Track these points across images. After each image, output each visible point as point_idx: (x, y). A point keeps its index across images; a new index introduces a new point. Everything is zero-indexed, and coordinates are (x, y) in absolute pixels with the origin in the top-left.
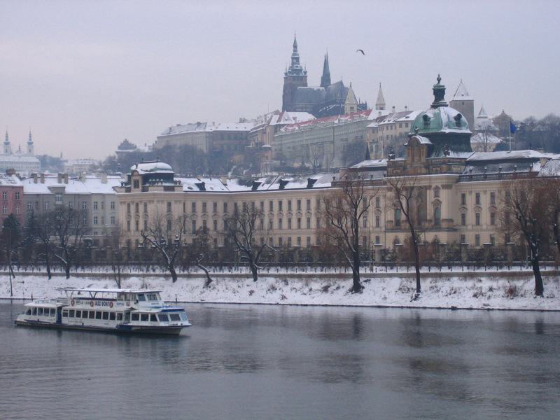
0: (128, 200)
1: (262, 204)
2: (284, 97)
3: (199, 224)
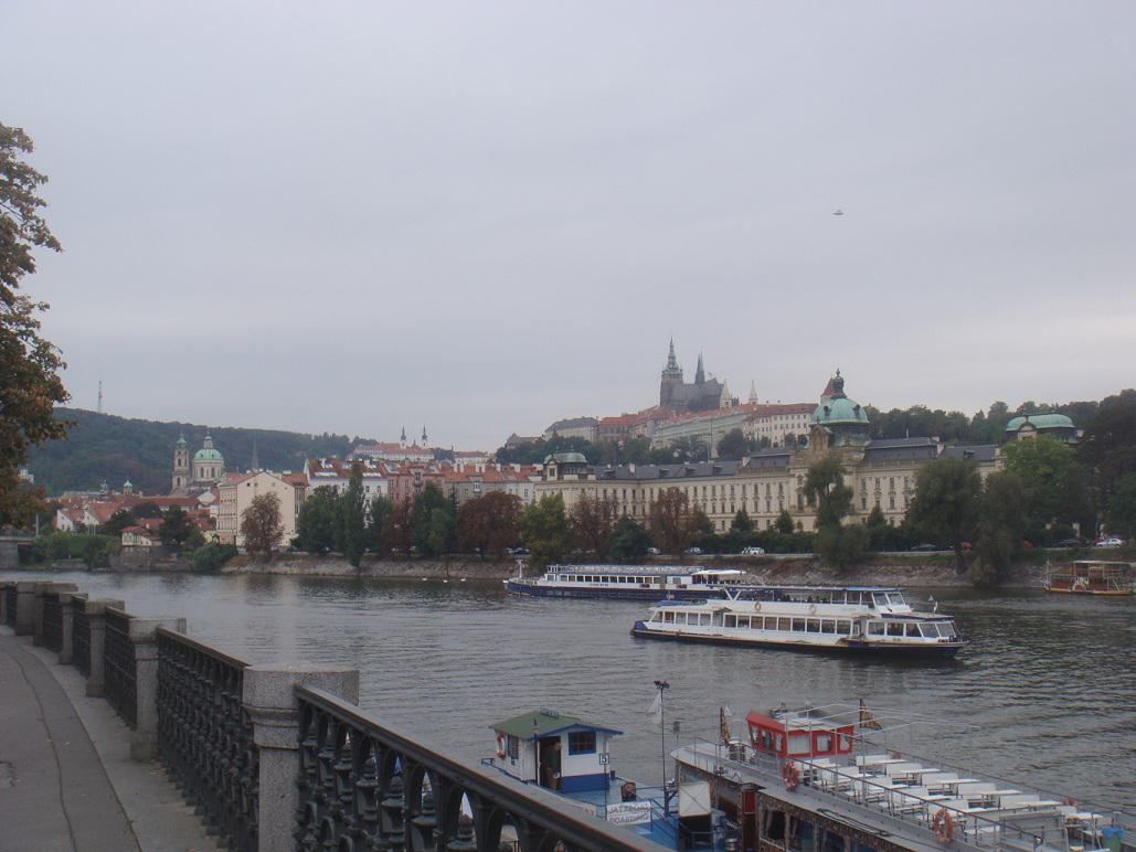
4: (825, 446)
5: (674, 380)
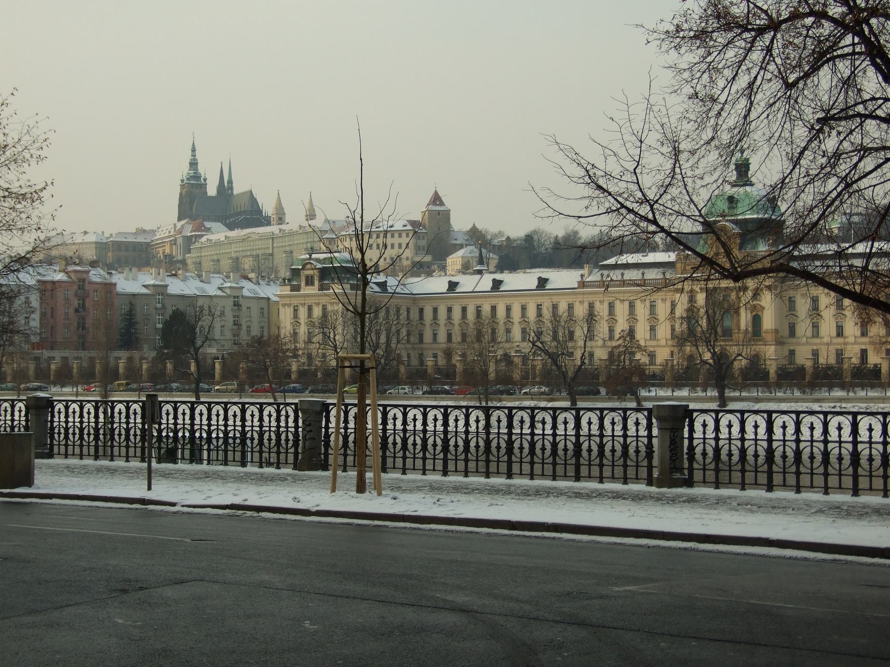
0: (295, 302)
1: (494, 308)
2: (180, 206)
3: (621, 325)
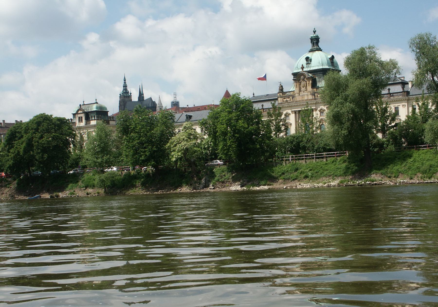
2: (119, 107)
4: (309, 88)
5: (127, 99)
